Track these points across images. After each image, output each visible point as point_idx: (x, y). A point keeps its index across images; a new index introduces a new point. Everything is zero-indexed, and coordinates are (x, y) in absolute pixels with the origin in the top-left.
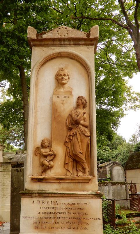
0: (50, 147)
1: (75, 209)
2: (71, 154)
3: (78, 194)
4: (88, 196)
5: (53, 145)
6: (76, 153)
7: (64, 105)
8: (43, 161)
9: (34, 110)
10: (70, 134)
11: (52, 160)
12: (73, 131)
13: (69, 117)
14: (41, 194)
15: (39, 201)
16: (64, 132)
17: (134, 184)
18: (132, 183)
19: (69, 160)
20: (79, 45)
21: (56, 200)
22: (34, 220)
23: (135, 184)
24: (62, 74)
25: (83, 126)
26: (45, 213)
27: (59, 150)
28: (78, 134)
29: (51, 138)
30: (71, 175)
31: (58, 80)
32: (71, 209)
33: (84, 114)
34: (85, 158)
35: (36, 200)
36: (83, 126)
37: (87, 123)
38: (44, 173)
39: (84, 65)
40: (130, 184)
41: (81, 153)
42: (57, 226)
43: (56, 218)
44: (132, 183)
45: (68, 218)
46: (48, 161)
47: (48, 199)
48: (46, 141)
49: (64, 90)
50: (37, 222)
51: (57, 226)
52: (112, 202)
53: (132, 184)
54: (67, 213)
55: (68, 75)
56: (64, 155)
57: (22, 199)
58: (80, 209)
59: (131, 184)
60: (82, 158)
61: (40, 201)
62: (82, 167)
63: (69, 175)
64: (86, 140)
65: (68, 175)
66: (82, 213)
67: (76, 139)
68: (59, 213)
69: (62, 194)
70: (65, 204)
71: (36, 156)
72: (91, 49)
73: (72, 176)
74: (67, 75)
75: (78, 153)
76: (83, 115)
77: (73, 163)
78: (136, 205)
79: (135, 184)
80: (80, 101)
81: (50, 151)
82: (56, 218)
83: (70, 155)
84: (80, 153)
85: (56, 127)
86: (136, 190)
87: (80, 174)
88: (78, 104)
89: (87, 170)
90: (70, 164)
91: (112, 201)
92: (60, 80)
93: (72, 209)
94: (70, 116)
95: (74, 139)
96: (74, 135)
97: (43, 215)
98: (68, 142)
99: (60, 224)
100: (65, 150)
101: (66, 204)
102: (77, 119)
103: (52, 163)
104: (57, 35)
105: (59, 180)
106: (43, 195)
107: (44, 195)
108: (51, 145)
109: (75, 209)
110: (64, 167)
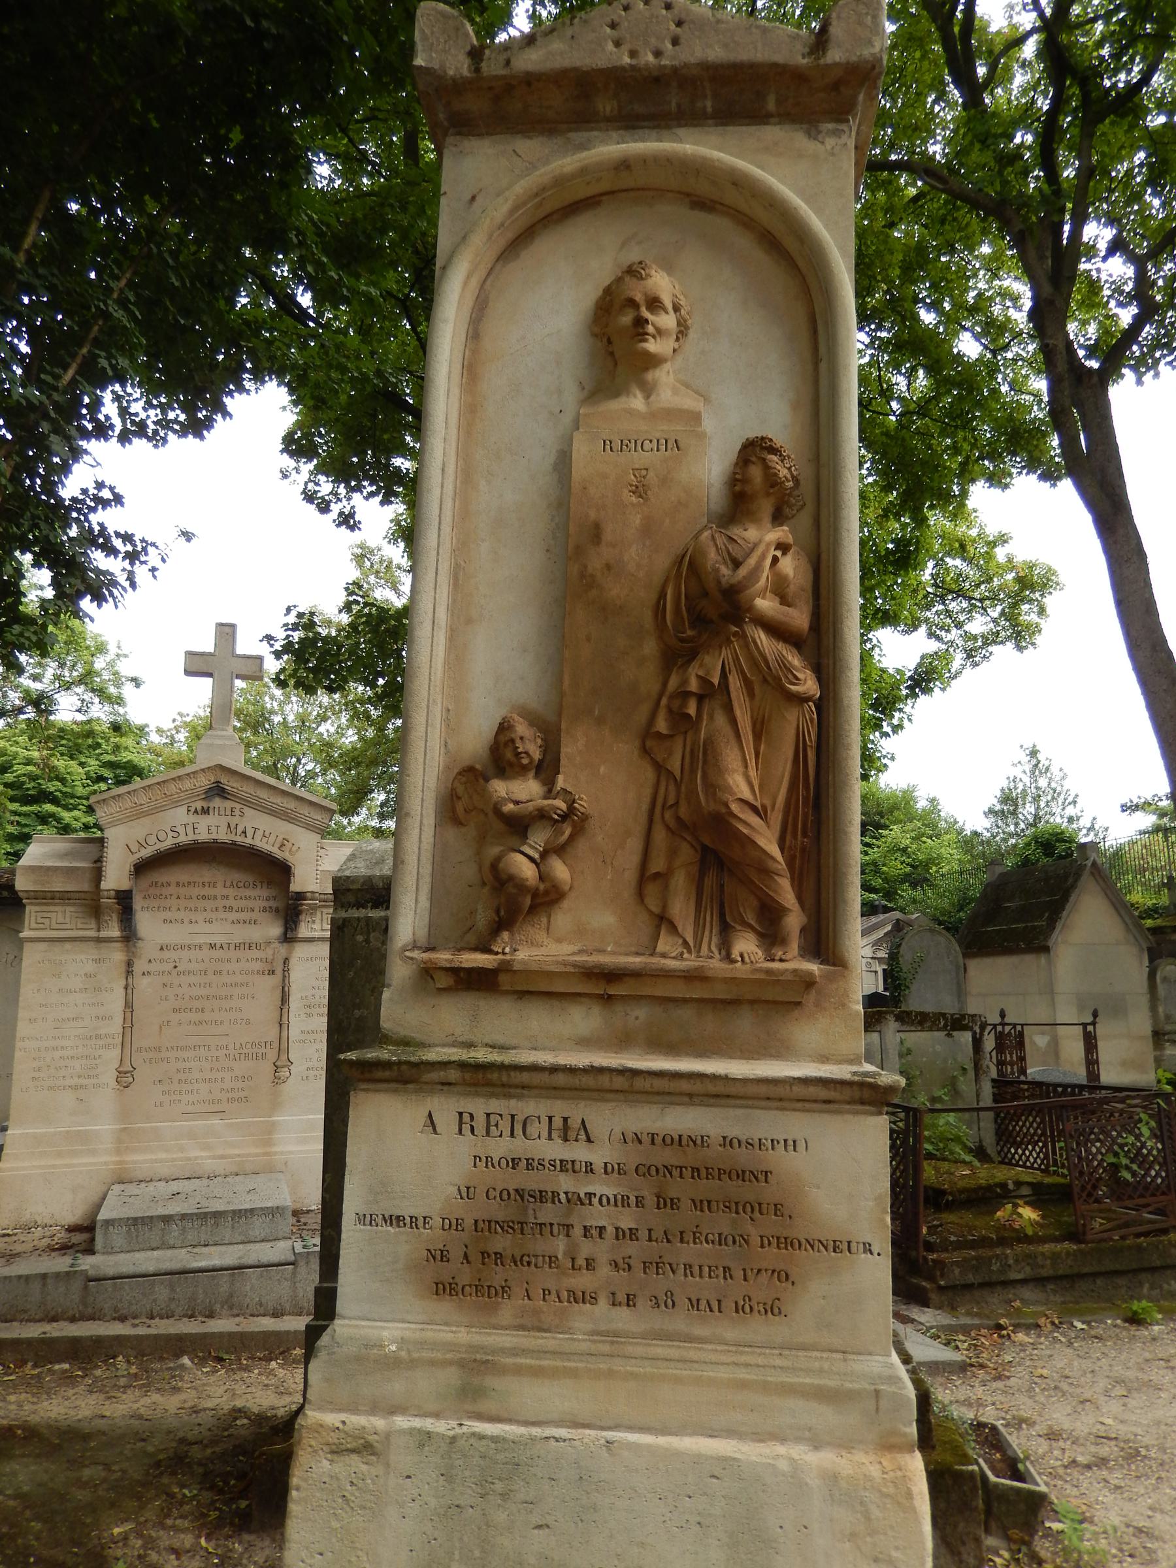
0: (547, 769)
1: (703, 1173)
2: (683, 811)
3: (726, 1079)
4: (798, 1090)
5: (571, 749)
6: (724, 810)
7: (646, 500)
8: (498, 859)
9: (447, 529)
10: (685, 682)
11: (560, 850)
12: (701, 665)
13: (679, 575)
14: (482, 1078)
15: (466, 1117)
16: (641, 667)
17: (1014, 1026)
18: (1007, 1020)
19: (672, 853)
20: (757, 117)
21: (577, 1111)
22: (432, 1235)
23: (1019, 1028)
24: (639, 297)
25: (776, 630)
26: (505, 1195)
27: (605, 782)
28: (735, 682)
29: (560, 715)
30: (682, 954)
31: (609, 342)
32: (676, 1173)
33: (779, 553)
35: (445, 1108)
36: (776, 630)
37: (799, 618)
38: (505, 935)
39: (790, 244)
40: (995, 1026)
42: (583, 1281)
43: (577, 1231)
44: (1007, 1020)
45: (658, 1233)
46: (537, 856)
47: (527, 1107)
48: (521, 728)
49: (648, 404)
50: (451, 1256)
51: (583, 1281)
52: (906, 1120)
53: (1003, 1024)
54: (650, 1200)
55: (676, 309)
56: (643, 819)
57: (353, 1099)
58: (741, 1175)
59: (999, 1028)
60: (761, 842)
61: (472, 1117)
62: (755, 903)
63: (671, 955)
64: (791, 724)
65: (661, 947)
66: (756, 1208)
67: (721, 720)
68: (595, 1201)
69: (554, 1069)
70: (640, 1142)
71: (461, 824)
72: (830, 142)
73: (686, 955)
74: (670, 307)
75: (735, 807)
76: (775, 560)
78: (1025, 1135)
79: (1019, 1028)
81: (550, 791)
82: (577, 1231)
83: (678, 819)
84: (746, 808)
86: (1022, 1059)
87: (746, 945)
88: (737, 488)
89: (794, 921)
90: (680, 881)
91: (907, 1116)
92: (618, 341)
93: (687, 1173)
94: (689, 566)
95: (711, 718)
96: (714, 693)
97: (497, 1210)
98: (674, 737)
99: (604, 1271)
100: (648, 792)
101: (646, 1139)
102: (733, 581)
103: (560, 870)
104: (610, 46)
105: (603, 984)
106: (495, 1075)
107: (504, 1079)
108: (559, 753)
109: (703, 1173)
110: (640, 895)
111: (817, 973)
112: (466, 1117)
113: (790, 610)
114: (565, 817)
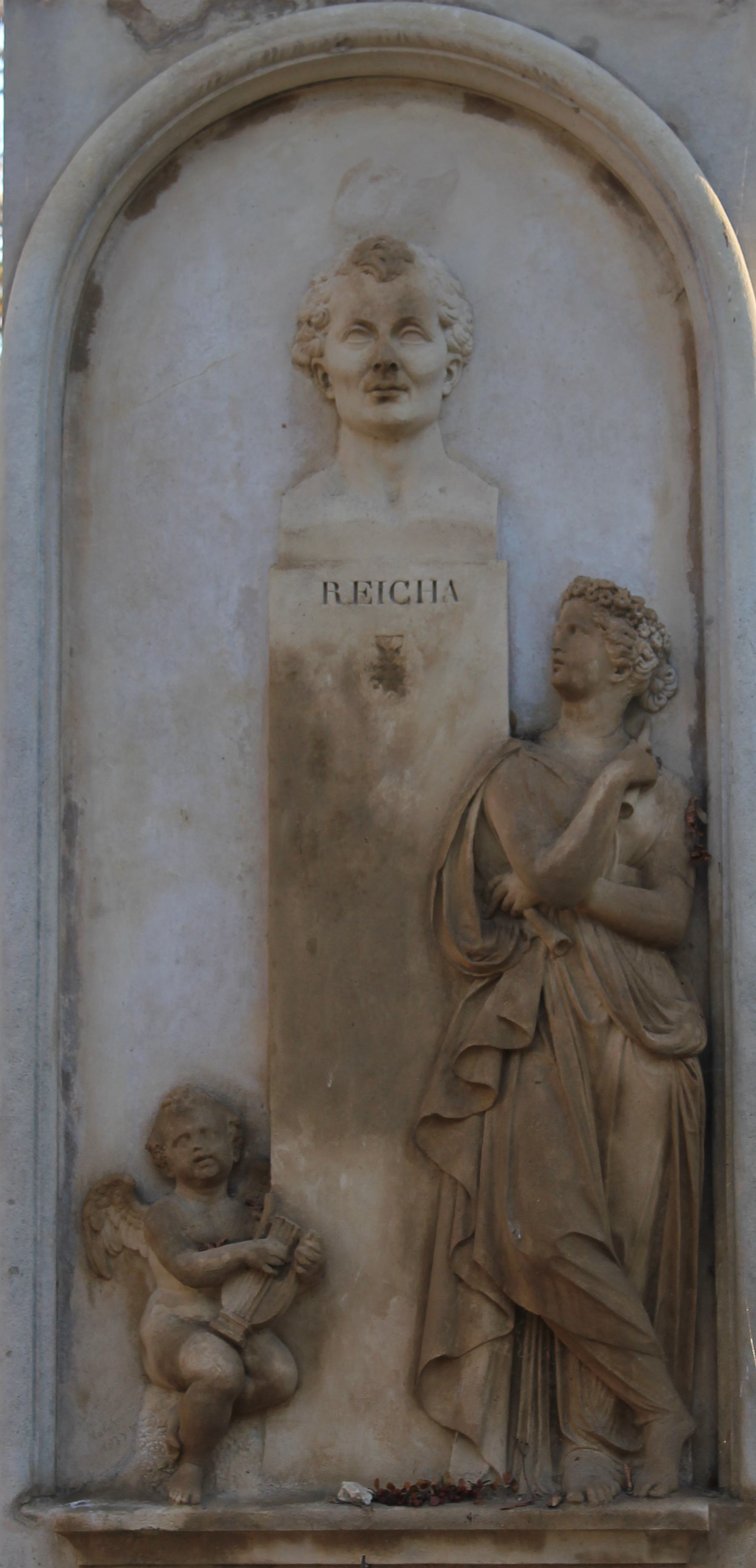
15: (331, 587)
34: (649, 1300)
37: (666, 906)
41: (601, 1247)
46: (238, 1339)
77: (516, 1349)
80: (594, 653)
85: (312, 948)
89: (665, 1431)
92: (378, 363)
111: (706, 1516)
112: (331, 587)
113: (649, 893)
114: (283, 1268)
